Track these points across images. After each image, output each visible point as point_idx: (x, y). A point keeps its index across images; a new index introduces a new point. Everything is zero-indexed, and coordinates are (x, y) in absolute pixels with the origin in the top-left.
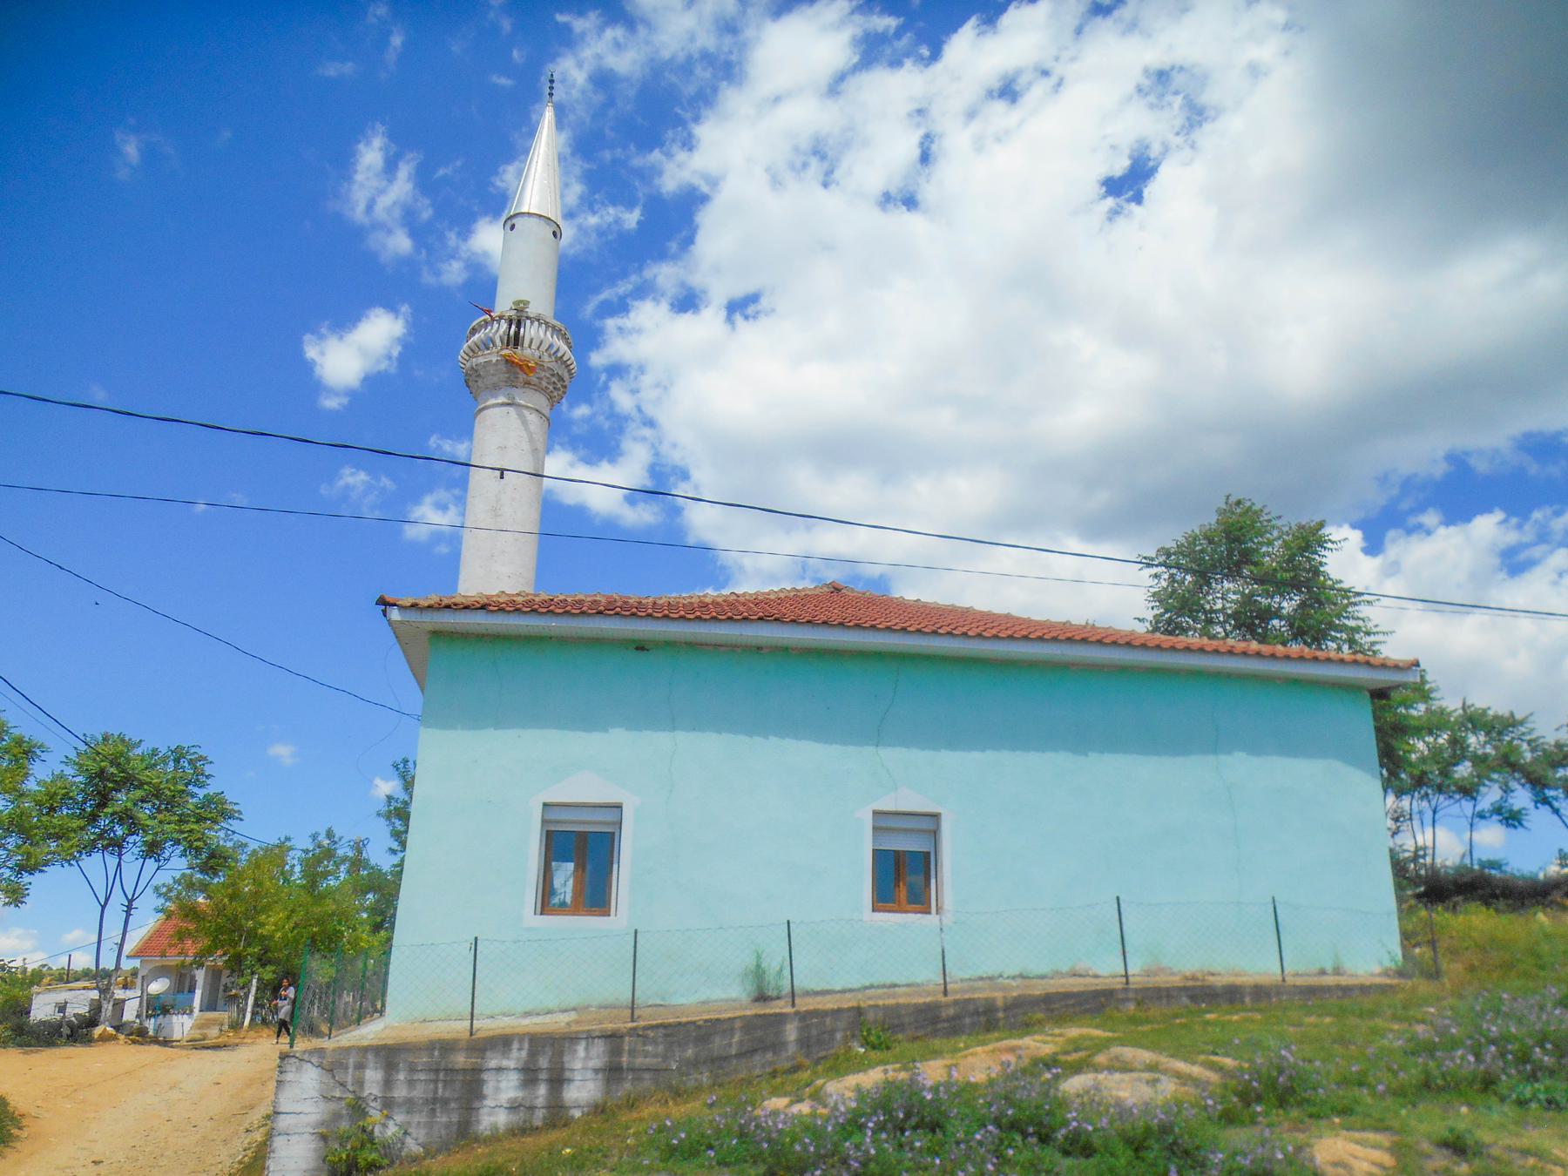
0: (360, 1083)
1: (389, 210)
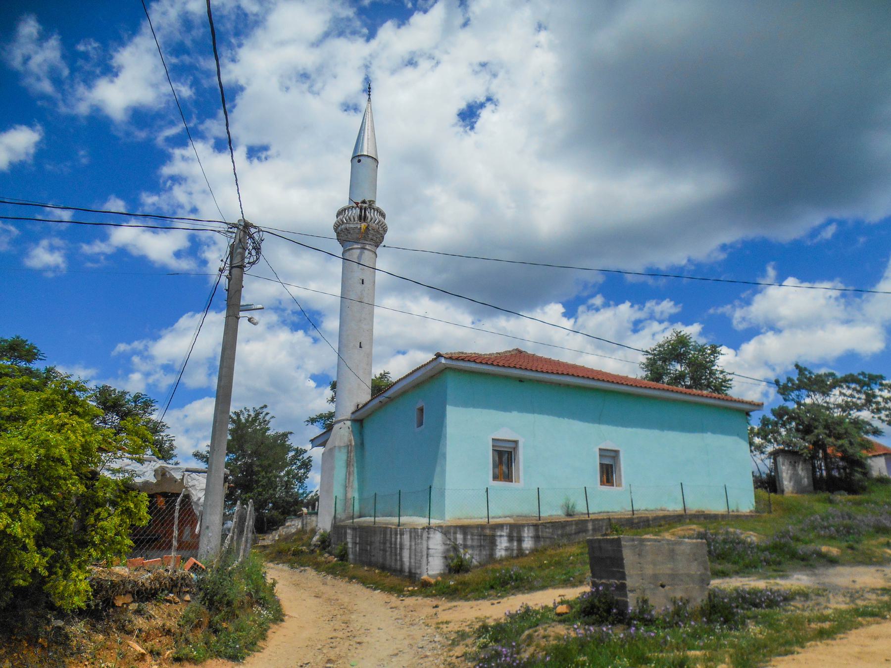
0: (456, 539)
1: (39, 65)
